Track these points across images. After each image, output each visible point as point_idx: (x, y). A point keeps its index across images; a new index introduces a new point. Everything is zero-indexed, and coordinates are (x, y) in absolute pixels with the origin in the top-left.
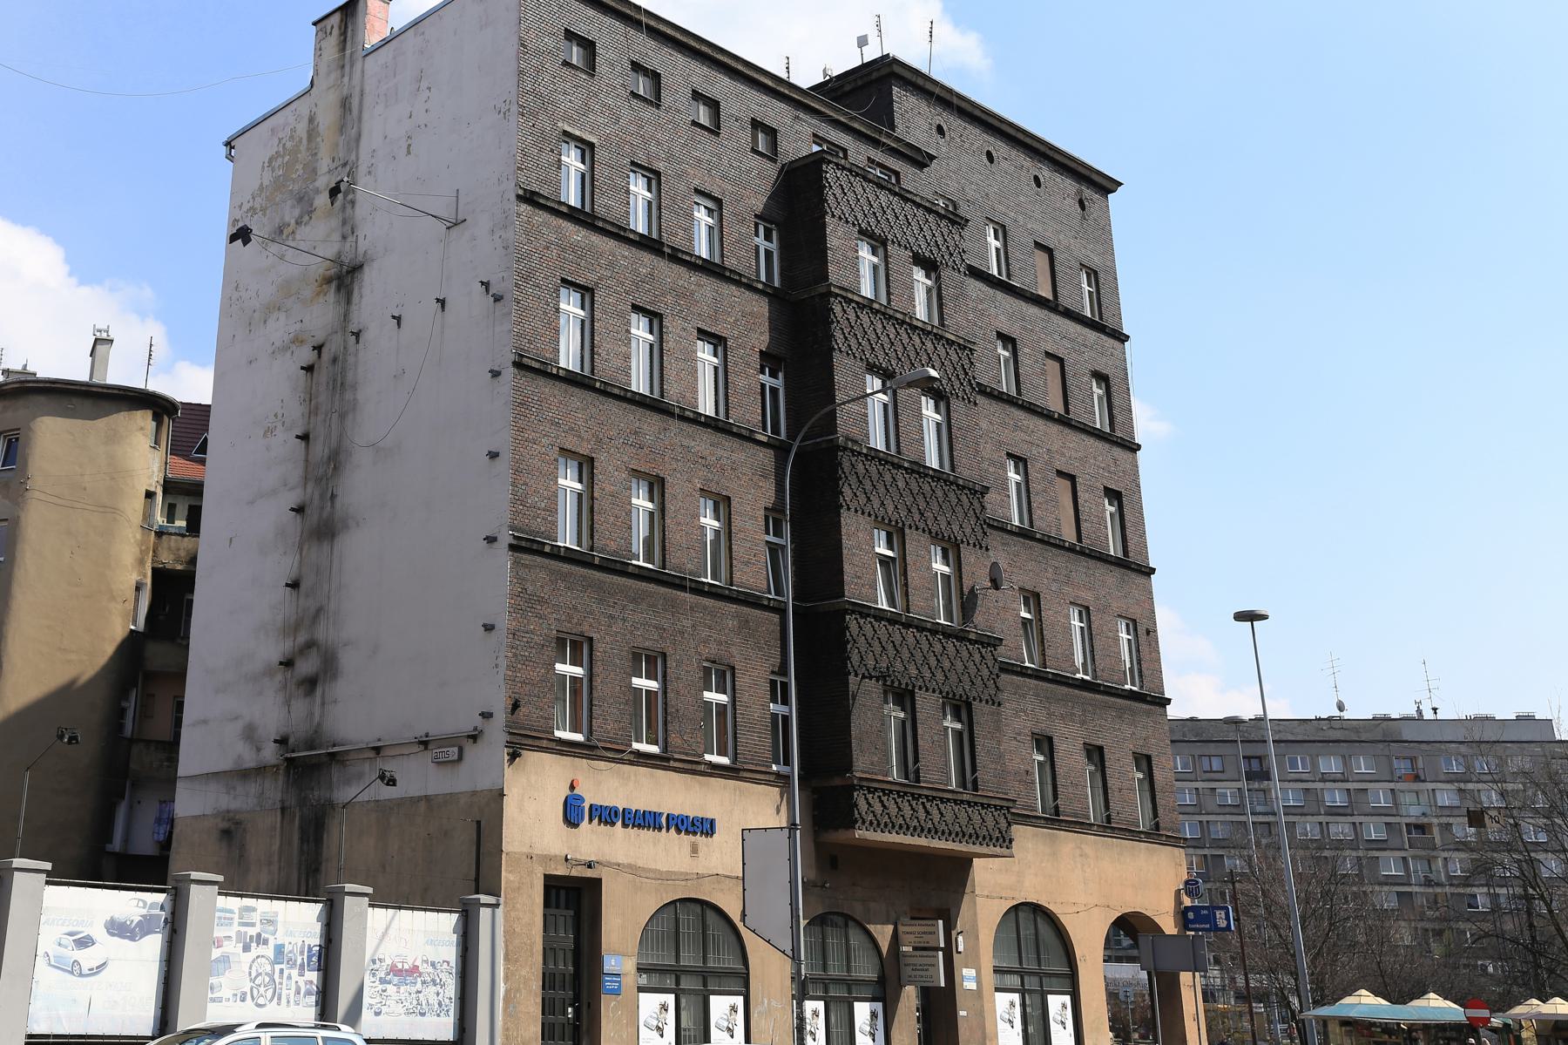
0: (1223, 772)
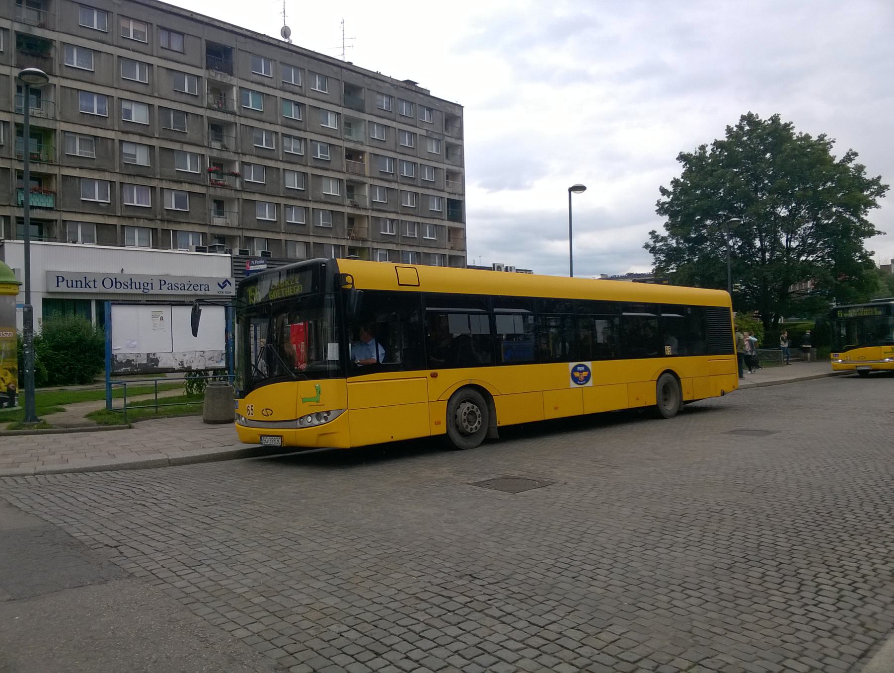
0: (183, 53)
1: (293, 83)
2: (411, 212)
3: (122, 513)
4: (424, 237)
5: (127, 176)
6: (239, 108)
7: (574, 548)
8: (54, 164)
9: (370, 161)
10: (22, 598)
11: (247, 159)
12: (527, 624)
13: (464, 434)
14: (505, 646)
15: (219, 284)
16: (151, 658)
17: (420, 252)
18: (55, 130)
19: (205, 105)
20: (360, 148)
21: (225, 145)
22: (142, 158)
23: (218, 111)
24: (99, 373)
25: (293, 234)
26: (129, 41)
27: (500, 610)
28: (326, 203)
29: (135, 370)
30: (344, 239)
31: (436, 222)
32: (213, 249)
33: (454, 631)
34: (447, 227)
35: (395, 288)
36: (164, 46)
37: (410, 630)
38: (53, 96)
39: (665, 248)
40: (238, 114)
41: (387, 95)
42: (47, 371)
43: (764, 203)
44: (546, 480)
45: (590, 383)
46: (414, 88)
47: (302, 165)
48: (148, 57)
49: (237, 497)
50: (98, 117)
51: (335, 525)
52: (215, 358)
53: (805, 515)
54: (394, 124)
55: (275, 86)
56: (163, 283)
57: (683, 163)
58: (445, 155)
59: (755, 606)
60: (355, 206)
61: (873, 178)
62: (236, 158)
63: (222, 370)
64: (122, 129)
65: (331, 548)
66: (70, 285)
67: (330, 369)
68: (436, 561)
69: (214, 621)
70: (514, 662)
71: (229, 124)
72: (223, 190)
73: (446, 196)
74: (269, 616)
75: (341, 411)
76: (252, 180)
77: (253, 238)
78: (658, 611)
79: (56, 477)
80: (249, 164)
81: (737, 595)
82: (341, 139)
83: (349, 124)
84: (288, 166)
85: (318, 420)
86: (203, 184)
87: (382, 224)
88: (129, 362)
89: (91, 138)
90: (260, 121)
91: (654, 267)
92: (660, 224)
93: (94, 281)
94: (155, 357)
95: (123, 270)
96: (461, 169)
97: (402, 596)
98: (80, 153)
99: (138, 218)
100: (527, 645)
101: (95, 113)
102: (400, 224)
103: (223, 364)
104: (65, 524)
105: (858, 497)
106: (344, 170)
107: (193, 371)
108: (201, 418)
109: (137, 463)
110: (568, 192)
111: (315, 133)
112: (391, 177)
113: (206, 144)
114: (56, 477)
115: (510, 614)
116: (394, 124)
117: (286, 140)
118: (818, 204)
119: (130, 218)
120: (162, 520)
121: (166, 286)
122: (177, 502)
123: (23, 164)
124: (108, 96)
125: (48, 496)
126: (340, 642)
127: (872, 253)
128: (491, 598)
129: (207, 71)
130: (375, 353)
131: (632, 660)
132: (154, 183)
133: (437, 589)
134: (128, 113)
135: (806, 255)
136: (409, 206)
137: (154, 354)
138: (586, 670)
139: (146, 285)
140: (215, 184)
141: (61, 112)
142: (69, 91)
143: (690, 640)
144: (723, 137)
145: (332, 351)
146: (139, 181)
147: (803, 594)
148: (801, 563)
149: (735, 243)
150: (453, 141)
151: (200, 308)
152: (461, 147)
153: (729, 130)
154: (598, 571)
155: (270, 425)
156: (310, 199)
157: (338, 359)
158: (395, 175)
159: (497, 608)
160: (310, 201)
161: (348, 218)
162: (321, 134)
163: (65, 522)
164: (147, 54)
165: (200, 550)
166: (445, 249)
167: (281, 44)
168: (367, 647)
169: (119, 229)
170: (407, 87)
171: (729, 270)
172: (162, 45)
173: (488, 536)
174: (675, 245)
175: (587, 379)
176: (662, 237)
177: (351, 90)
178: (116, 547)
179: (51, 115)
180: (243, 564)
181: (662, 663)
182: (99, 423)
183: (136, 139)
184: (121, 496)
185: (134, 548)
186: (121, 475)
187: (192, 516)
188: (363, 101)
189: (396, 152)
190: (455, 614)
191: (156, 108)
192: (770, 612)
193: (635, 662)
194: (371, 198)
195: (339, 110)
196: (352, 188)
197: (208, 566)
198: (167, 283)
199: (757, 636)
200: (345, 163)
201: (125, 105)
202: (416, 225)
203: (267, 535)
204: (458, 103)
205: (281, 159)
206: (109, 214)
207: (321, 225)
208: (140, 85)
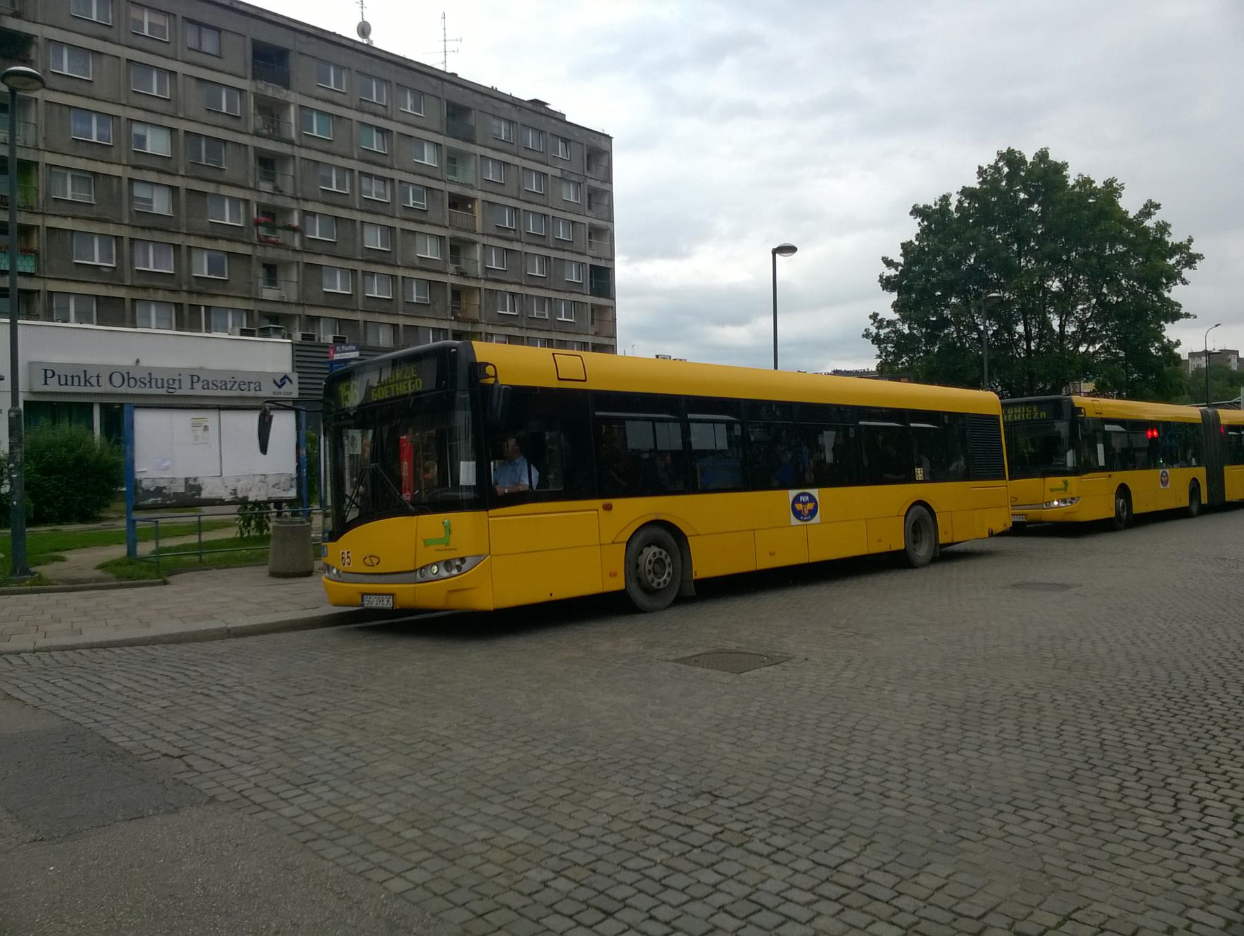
0: (219, 57)
1: (375, 101)
2: (539, 283)
3: (176, 708)
5: (139, 229)
6: (300, 134)
7: (844, 751)
8: (36, 211)
9: (483, 209)
10: (54, 837)
11: (309, 207)
12: (811, 865)
13: (648, 591)
14: (789, 898)
15: (275, 382)
16: (268, 926)
17: (552, 340)
18: (37, 163)
19: (251, 130)
20: (469, 193)
22: (161, 204)
23: (269, 138)
24: (107, 506)
25: (375, 312)
26: (143, 38)
27: (766, 844)
29: (168, 502)
30: (446, 320)
31: (575, 297)
32: (265, 332)
33: (709, 877)
34: (589, 305)
35: (553, 383)
36: (193, 47)
37: (646, 876)
38: (34, 115)
39: (893, 335)
41: (506, 120)
42: (32, 505)
43: (1029, 273)
44: (778, 655)
45: (817, 519)
46: (543, 111)
47: (387, 216)
48: (170, 61)
49: (342, 681)
50: (98, 146)
51: (495, 722)
52: (282, 485)
53: (1153, 701)
54: (517, 161)
55: (349, 104)
56: (195, 379)
57: (919, 220)
58: (587, 204)
59: (1122, 832)
60: (462, 274)
61: (1181, 243)
63: (290, 502)
64: (134, 163)
65: (497, 755)
66: (63, 382)
67: (464, 498)
68: (653, 772)
69: (353, 867)
70: (808, 922)
71: (284, 158)
74: (432, 858)
75: (479, 558)
76: (318, 237)
77: (318, 318)
78: (989, 842)
79: (66, 655)
80: (313, 214)
81: (1092, 816)
83: (453, 159)
84: (368, 218)
85: (448, 571)
86: (248, 241)
87: (499, 299)
88: (159, 491)
89: (87, 175)
90: (328, 153)
91: (879, 361)
92: (885, 304)
93: (98, 376)
94: (197, 484)
95: (138, 361)
96: (609, 223)
97: (617, 826)
98: (73, 196)
99: (156, 289)
100: (820, 896)
101: (95, 139)
102: (524, 298)
103: (292, 494)
104: (97, 724)
105: (1215, 675)
106: (447, 224)
107: (251, 503)
108: (266, 569)
109: (183, 633)
110: (771, 255)
111: (406, 172)
112: (511, 235)
113: (251, 185)
114: (66, 655)
115: (783, 849)
116: (517, 161)
117: (365, 180)
118: (1102, 273)
119: (145, 288)
120: (238, 716)
121: (200, 384)
122: (254, 689)
124: (112, 116)
125: (61, 683)
126: (547, 896)
127: (1178, 344)
128: (748, 826)
129: (253, 83)
130: (526, 477)
131: (975, 915)
132: (177, 240)
133: (669, 815)
134: (141, 140)
135: (1086, 345)
137: (195, 479)
138: (914, 932)
139: (171, 382)
140: (264, 242)
141: (45, 139)
142: (57, 108)
143: (1047, 883)
144: (974, 182)
145: (467, 473)
146: (158, 236)
147: (1183, 813)
148: (1169, 769)
149: (990, 328)
151: (272, 413)
152: (610, 193)
153: (981, 171)
154: (888, 784)
155: (376, 578)
156: (399, 263)
157: (475, 484)
158: (518, 231)
159: (761, 840)
161: (452, 291)
162: (414, 174)
163: (96, 721)
164: (167, 58)
165: (306, 759)
166: (588, 334)
167: (358, 47)
168: (590, 902)
169: (128, 304)
170: (535, 108)
171: (986, 364)
172: (189, 46)
173: (717, 735)
174: (906, 331)
175: (813, 513)
176: (888, 321)
178: (180, 757)
179: (30, 142)
180: (375, 779)
181: (1018, 917)
182: (119, 577)
183: (152, 177)
184: (170, 682)
185: (209, 759)
186: (160, 651)
187: (280, 710)
188: (473, 128)
189: (518, 199)
190: (535, 832)
191: (181, 134)
192: (1145, 840)
193: (979, 918)
194: (484, 263)
195: (439, 139)
196: (457, 248)
197: (325, 783)
198: (201, 380)
199: (1139, 876)
201: (137, 129)
202: (547, 300)
203: (398, 737)
204: (606, 133)
205: (358, 207)
206: (114, 282)
207: (415, 301)
208: (157, 101)
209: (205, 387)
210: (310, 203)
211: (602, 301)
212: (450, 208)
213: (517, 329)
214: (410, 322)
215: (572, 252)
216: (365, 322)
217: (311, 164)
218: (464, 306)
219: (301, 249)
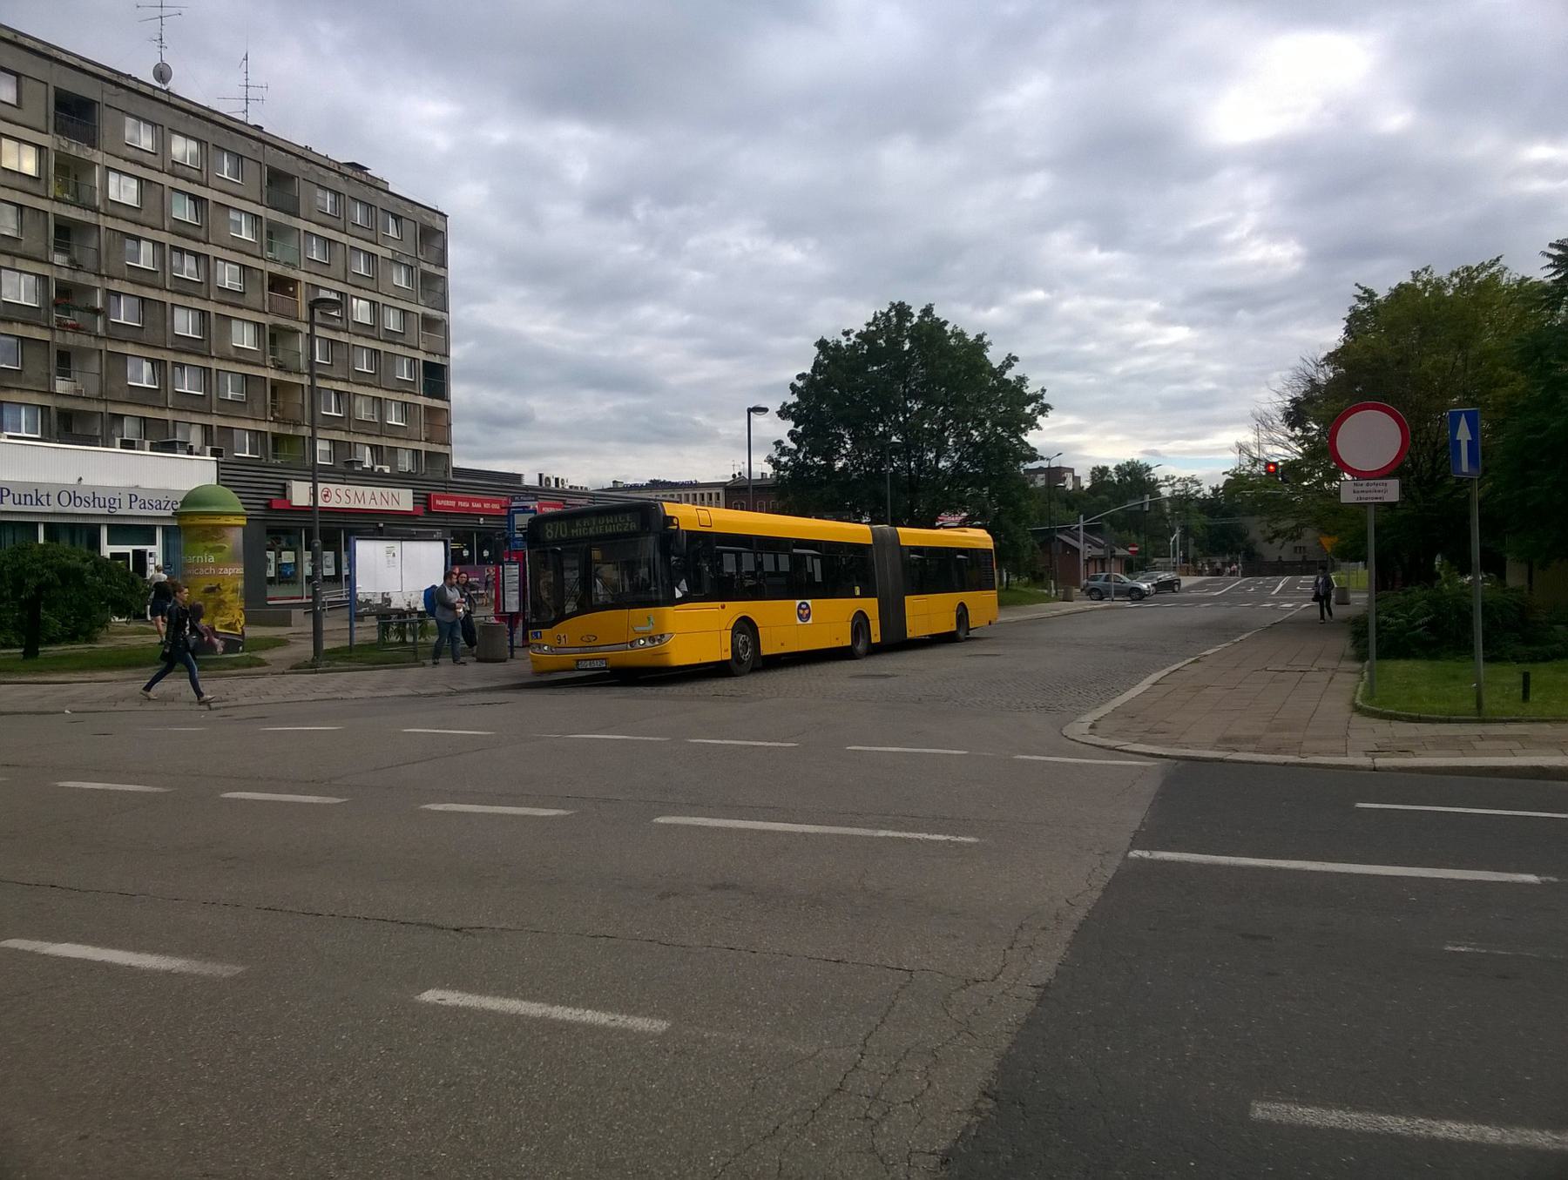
4: (389, 422)
11: (115, 286)
20: (292, 274)
21: (75, 261)
28: (238, 361)
30: (265, 421)
31: (407, 398)
40: (102, 211)
45: (810, 621)
46: (364, 178)
54: (344, 238)
56: (133, 498)
62: (95, 282)
72: (76, 335)
73: (421, 356)
76: (122, 321)
80: (118, 294)
82: (262, 258)
83: (273, 233)
84: (179, 300)
86: (45, 325)
90: (136, 223)
93: (48, 495)
95: (80, 479)
96: (444, 314)
111: (223, 247)
116: (344, 238)
123: (1102, 550)
136: (365, 370)
139: (112, 501)
140: (63, 327)
150: (432, 269)
156: (213, 354)
160: (213, 357)
162: (231, 250)
175: (808, 616)
177: (278, 179)
189: (346, 283)
200: (266, 297)
207: (230, 398)
209: (142, 506)
210: (116, 281)
211: (437, 403)
212: (269, 290)
213: (343, 433)
214: (224, 423)
215: (404, 345)
216: (175, 421)
217: (117, 236)
218: (281, 404)
219: (104, 335)
